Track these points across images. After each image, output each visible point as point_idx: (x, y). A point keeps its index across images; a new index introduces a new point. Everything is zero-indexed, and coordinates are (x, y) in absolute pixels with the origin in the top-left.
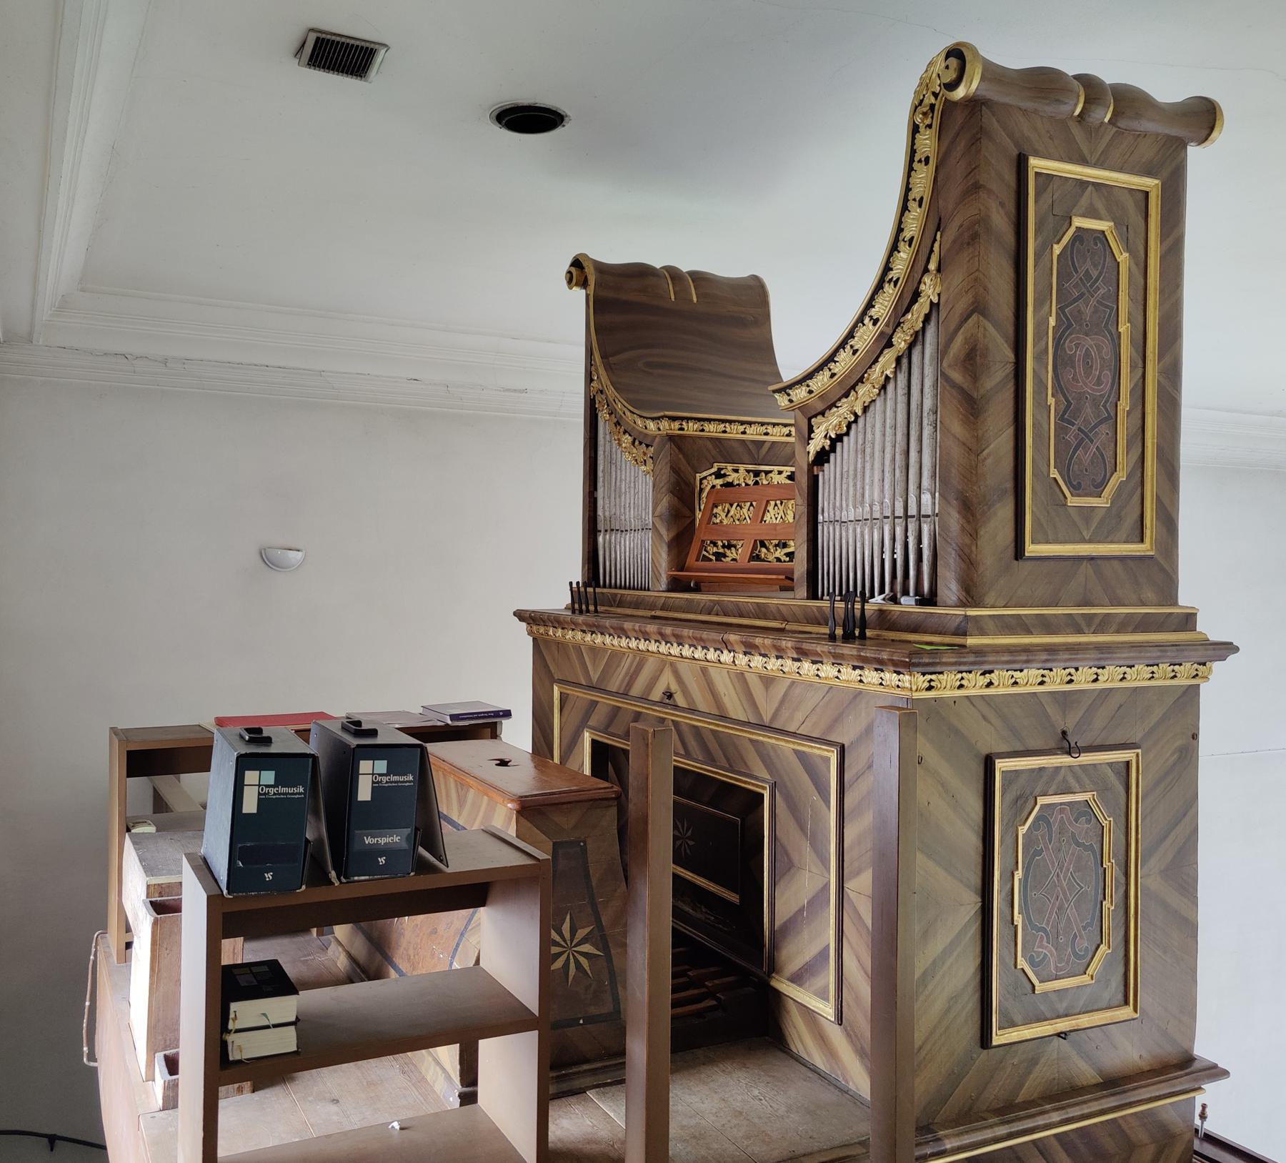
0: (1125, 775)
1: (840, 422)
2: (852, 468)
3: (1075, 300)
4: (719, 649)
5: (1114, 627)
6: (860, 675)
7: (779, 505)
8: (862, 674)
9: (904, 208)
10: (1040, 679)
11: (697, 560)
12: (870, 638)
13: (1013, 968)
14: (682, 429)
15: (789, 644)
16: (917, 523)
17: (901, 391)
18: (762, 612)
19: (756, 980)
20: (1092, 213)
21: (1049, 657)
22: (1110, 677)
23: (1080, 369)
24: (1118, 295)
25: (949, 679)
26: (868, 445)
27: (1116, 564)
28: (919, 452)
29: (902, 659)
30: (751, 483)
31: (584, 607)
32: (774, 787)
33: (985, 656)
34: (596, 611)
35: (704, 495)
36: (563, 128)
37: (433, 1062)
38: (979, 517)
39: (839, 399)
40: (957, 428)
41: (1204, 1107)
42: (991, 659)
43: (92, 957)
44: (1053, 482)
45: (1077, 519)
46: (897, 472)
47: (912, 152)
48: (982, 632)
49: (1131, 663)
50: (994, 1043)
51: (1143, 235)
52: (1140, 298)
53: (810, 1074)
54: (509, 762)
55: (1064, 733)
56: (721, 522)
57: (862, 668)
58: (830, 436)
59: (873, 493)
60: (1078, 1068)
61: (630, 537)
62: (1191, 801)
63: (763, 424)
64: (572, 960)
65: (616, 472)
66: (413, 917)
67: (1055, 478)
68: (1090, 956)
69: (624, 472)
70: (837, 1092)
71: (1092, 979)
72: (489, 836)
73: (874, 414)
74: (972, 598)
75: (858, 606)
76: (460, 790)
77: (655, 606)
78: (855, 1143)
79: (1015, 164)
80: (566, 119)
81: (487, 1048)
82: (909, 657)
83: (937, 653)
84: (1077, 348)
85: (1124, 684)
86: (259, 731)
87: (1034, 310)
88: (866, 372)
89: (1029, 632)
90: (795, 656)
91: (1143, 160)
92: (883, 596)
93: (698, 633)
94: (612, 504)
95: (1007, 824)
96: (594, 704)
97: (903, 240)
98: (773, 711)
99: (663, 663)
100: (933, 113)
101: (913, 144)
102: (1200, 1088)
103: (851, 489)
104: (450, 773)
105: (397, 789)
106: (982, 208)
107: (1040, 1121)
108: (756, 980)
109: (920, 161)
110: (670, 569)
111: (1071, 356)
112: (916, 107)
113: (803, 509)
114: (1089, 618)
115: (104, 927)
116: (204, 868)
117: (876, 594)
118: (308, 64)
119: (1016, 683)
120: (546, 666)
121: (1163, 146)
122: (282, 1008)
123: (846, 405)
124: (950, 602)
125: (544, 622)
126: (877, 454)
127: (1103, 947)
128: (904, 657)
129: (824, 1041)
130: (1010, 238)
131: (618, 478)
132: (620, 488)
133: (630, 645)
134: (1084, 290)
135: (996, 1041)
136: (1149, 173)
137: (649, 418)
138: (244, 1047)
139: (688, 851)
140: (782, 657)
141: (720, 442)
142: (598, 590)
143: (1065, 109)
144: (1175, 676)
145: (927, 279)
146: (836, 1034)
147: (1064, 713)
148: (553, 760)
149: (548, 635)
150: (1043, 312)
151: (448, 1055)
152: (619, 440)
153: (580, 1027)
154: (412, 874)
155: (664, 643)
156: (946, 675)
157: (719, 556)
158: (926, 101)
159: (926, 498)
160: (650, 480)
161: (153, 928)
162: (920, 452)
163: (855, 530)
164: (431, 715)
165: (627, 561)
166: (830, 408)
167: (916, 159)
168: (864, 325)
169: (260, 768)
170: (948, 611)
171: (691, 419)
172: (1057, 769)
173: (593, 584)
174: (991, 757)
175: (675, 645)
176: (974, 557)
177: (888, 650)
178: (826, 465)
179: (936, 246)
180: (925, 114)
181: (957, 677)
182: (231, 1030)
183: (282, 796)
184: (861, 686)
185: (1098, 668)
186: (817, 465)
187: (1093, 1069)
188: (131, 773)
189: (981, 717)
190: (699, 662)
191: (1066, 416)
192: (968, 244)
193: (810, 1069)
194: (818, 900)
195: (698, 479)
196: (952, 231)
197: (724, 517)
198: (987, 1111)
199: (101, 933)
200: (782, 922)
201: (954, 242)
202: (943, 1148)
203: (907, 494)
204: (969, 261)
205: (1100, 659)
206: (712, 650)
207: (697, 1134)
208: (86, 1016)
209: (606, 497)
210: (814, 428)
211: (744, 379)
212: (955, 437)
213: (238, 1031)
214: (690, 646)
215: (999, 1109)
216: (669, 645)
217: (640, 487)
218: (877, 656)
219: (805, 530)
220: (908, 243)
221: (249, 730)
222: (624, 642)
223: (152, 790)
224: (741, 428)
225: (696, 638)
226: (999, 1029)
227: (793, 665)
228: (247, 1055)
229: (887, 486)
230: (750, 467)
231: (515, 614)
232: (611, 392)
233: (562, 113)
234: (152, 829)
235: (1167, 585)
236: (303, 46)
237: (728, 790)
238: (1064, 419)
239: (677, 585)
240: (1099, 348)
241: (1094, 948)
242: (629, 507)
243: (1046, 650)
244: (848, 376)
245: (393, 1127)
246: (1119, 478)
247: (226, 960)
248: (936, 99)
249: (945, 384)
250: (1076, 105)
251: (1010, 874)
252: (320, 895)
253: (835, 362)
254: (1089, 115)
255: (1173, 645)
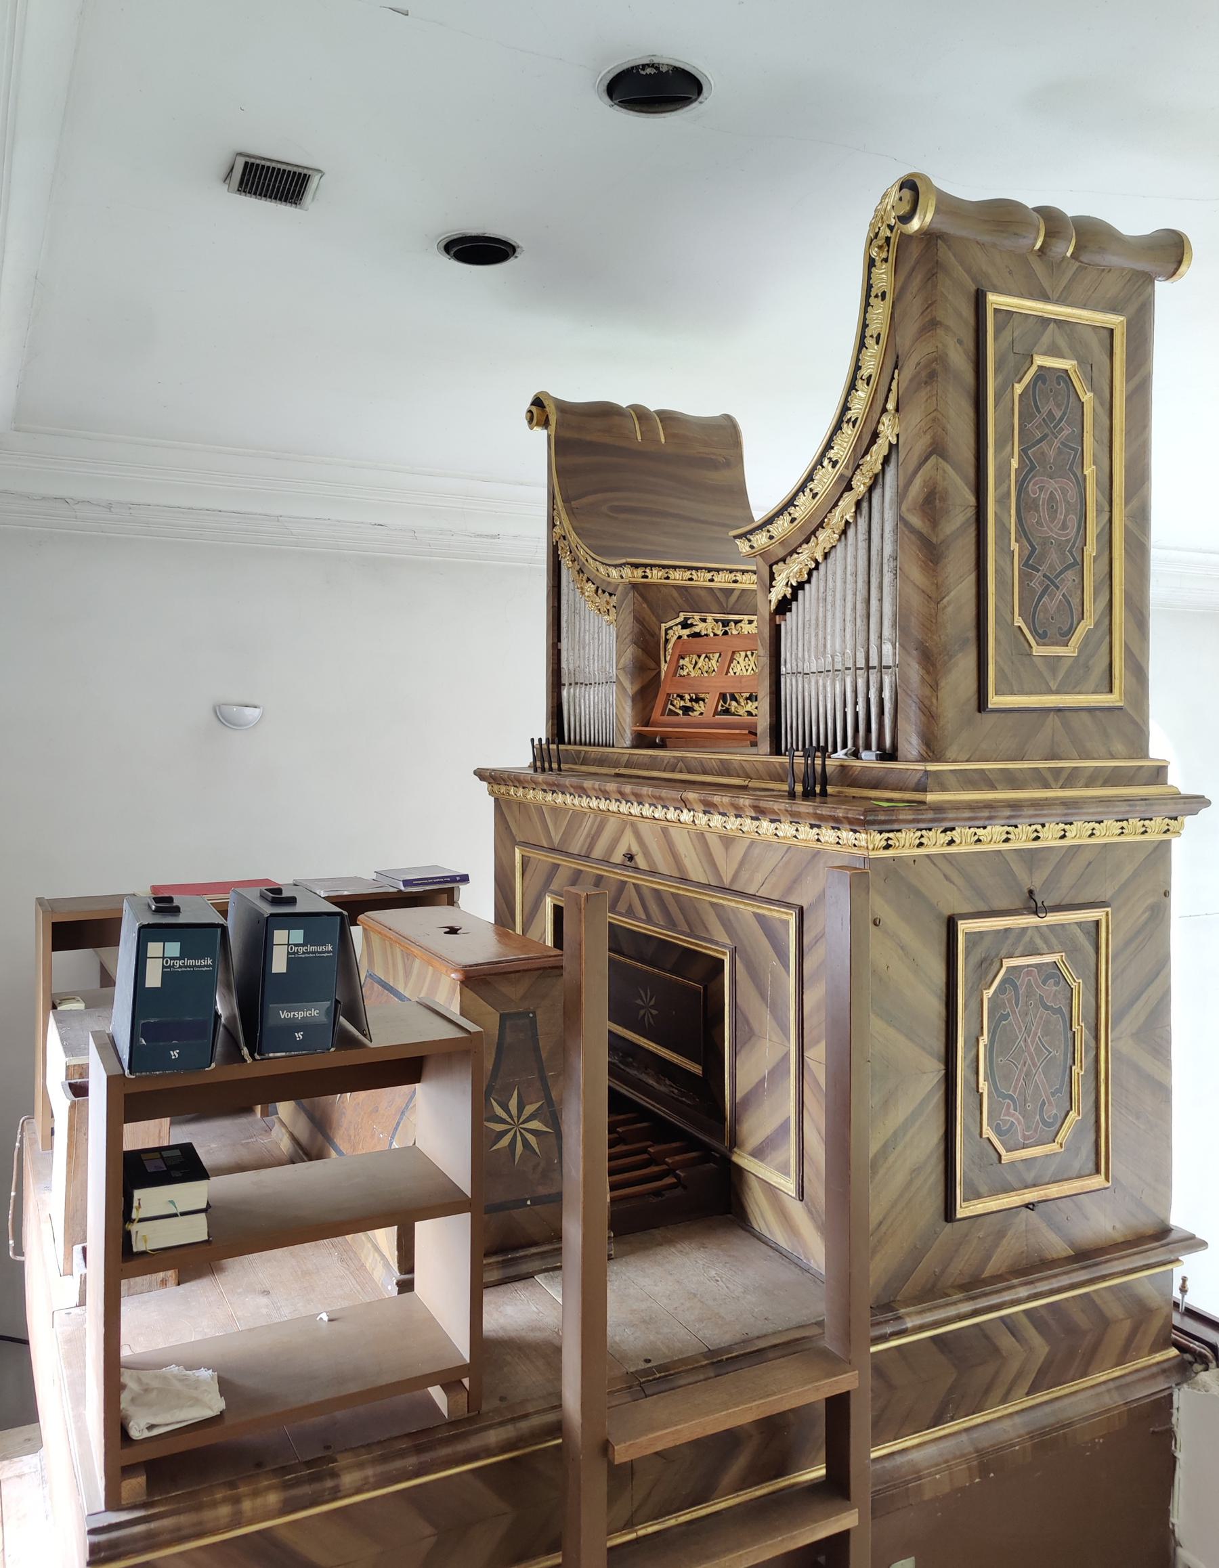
0: (1095, 936)
1: (801, 569)
2: (813, 617)
3: (1040, 441)
4: (678, 808)
5: (1082, 782)
6: (818, 834)
7: (750, 656)
8: (820, 832)
9: (862, 345)
10: (1004, 836)
11: (663, 714)
12: (832, 795)
13: (978, 1137)
14: (646, 577)
15: (747, 802)
16: (879, 673)
17: (862, 536)
18: (725, 769)
19: (717, 1155)
20: (1054, 352)
21: (1013, 813)
22: (1078, 833)
23: (1044, 513)
24: (1083, 437)
25: (907, 838)
26: (829, 593)
27: (1084, 715)
28: (879, 600)
29: (858, 817)
30: (720, 633)
31: (546, 765)
32: (734, 951)
33: (945, 813)
34: (560, 769)
35: (670, 646)
36: (516, 260)
37: (372, 1249)
38: (939, 667)
39: (800, 545)
40: (916, 574)
41: (1184, 1280)
42: (951, 815)
43: (17, 1144)
44: (1017, 629)
45: (1043, 668)
46: (859, 620)
47: (869, 287)
48: (944, 788)
49: (1099, 819)
50: (959, 1216)
51: (1108, 374)
52: (1106, 441)
53: (771, 1253)
54: (459, 929)
55: (1031, 892)
56: (688, 674)
57: (819, 827)
58: (791, 584)
59: (834, 643)
60: (1048, 1240)
61: (594, 691)
62: (1162, 964)
63: (731, 571)
64: (519, 1138)
65: (580, 622)
66: (354, 1094)
67: (1019, 627)
68: (1059, 1124)
69: (587, 623)
70: (797, 1271)
71: (1061, 1147)
72: (424, 1009)
73: (835, 560)
74: (933, 752)
75: (818, 761)
76: (406, 960)
77: (619, 763)
78: (812, 1324)
79: (973, 300)
80: (518, 250)
81: (424, 1230)
82: (863, 815)
83: (893, 810)
84: (1041, 491)
85: (1092, 841)
86: (170, 900)
87: (995, 452)
88: (826, 517)
89: (992, 787)
90: (753, 815)
91: (1108, 296)
92: (845, 751)
93: (657, 792)
94: (577, 655)
95: (971, 988)
96: (556, 867)
97: (861, 378)
98: (733, 873)
99: (625, 823)
100: (889, 247)
101: (869, 278)
102: (1177, 1260)
103: (813, 640)
104: (396, 942)
105: (317, 960)
106: (940, 345)
107: (1007, 1296)
108: (717, 1155)
109: (876, 296)
110: (635, 725)
111: (1034, 500)
112: (872, 240)
113: (765, 660)
114: (1057, 772)
115: (31, 1113)
116: (108, 1045)
117: (839, 748)
118: (238, 190)
119: (979, 841)
120: (508, 828)
121: (1129, 280)
122: (192, 1194)
123: (807, 551)
124: (911, 757)
125: (504, 781)
126: (838, 603)
127: (1072, 1114)
128: (859, 815)
129: (785, 1217)
130: (969, 377)
131: (582, 629)
132: (584, 639)
133: (591, 805)
134: (1047, 431)
135: (961, 1213)
136: (1113, 309)
137: (612, 565)
138: (147, 1237)
139: (651, 1020)
140: (740, 816)
141: (687, 591)
142: (561, 747)
143: (1024, 242)
144: (1146, 832)
145: (885, 419)
146: (797, 1209)
147: (1031, 873)
148: (515, 931)
149: (509, 795)
150: (1004, 454)
151: (385, 1238)
152: (582, 588)
153: (528, 1208)
154: (333, 1049)
155: (624, 802)
156: (904, 833)
157: (687, 710)
158: (881, 234)
159: (887, 648)
160: (613, 630)
161: (70, 1111)
162: (881, 600)
163: (817, 682)
164: (385, 881)
165: (592, 716)
166: (791, 554)
167: (873, 294)
168: (823, 467)
169: (164, 940)
170: (909, 766)
171: (655, 566)
172: (1024, 930)
173: (556, 739)
174: (953, 918)
175: (635, 804)
176: (935, 709)
177: (844, 807)
178: (788, 614)
179: (894, 384)
180: (880, 247)
181: (916, 835)
182: (134, 1220)
183: (188, 969)
184: (819, 845)
185: (1066, 824)
186: (779, 614)
187: (1064, 1241)
188: (57, 946)
189: (942, 877)
190: (659, 822)
191: (1030, 562)
192: (926, 383)
193: (771, 1247)
194: (778, 1070)
195: (663, 629)
196: (908, 371)
197: (691, 669)
198: (953, 1287)
199: (28, 1119)
200: (743, 1094)
201: (911, 380)
202: (904, 1327)
203: (868, 645)
204: (927, 400)
205: (1066, 815)
206: (672, 809)
207: (647, 1319)
208: (11, 1208)
209: (570, 649)
210: (775, 576)
211: (713, 524)
212: (915, 584)
213: (141, 1220)
214: (676, 809)
215: (963, 1284)
216: (629, 804)
217: (604, 638)
218: (833, 814)
219: (767, 683)
220: (866, 381)
221: (157, 900)
222: (585, 801)
223: (99, 968)
224: (709, 576)
225: (655, 797)
226: (964, 1201)
227: (752, 823)
228: (151, 1246)
229: (848, 636)
230: (718, 616)
231: (475, 773)
232: (573, 538)
233: (514, 244)
234: (80, 1006)
235: (1138, 739)
236: (231, 170)
237: (690, 956)
238: (1029, 564)
239: (642, 741)
240: (1064, 492)
241: (1063, 1114)
242: (594, 659)
243: (1010, 806)
244: (808, 521)
245: (321, 1319)
246: (1086, 626)
247: (128, 1146)
248: (892, 231)
249: (904, 529)
250: (1036, 239)
251: (974, 1040)
252: (235, 1072)
253: (795, 506)
254: (1051, 249)
255: (1142, 800)
